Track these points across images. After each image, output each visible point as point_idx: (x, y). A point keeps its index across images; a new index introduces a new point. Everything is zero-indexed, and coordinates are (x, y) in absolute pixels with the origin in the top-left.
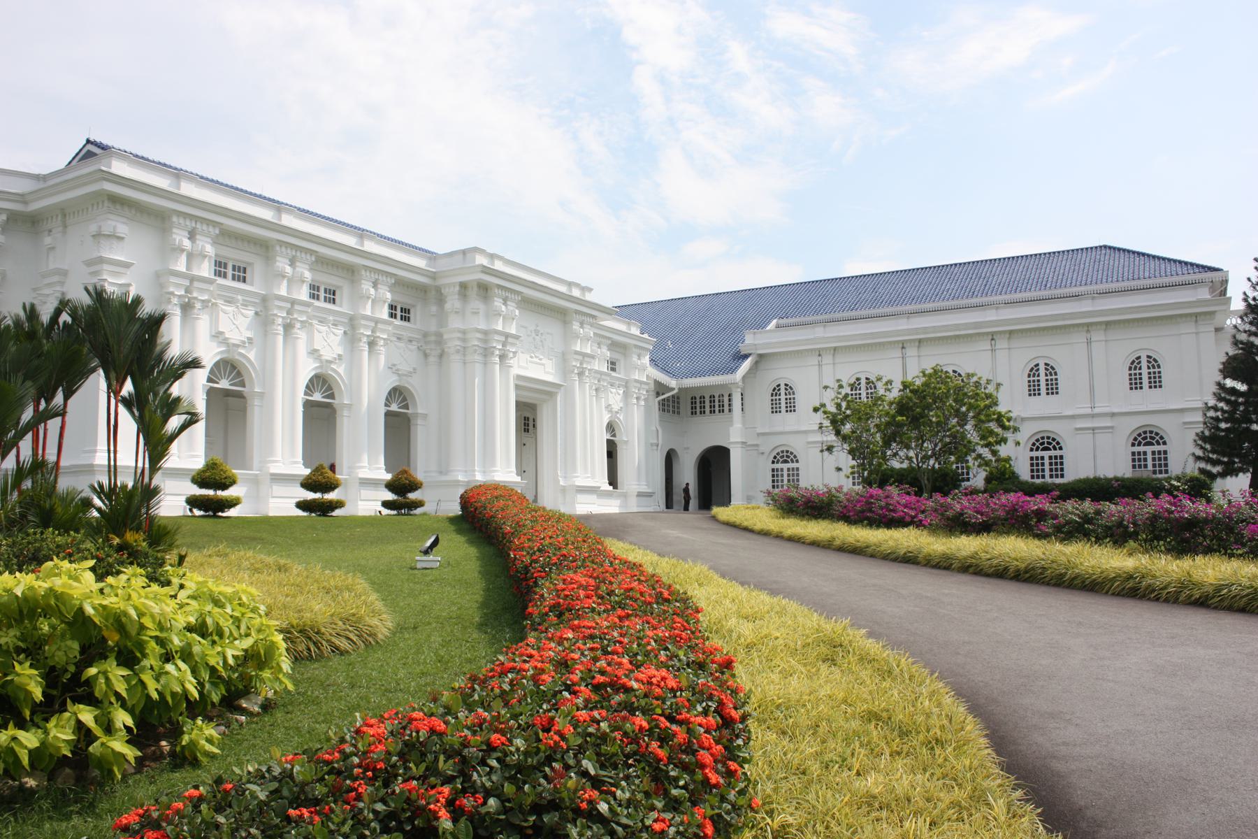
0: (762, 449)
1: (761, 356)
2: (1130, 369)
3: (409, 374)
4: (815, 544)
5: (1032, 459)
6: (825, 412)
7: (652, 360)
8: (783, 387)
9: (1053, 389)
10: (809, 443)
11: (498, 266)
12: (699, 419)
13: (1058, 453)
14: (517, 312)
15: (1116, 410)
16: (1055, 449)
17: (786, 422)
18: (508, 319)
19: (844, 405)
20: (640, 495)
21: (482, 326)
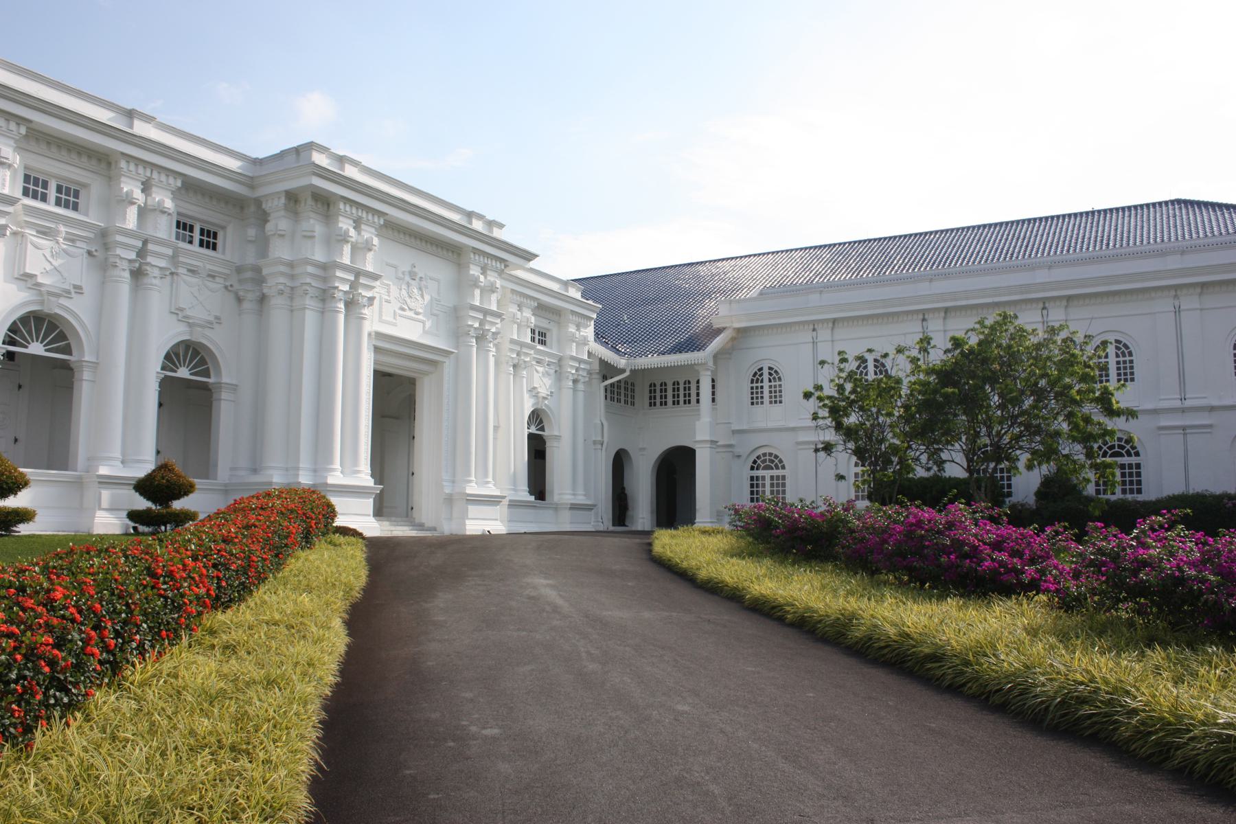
0: (737, 450)
1: (739, 330)
2: (752, 382)
3: (209, 325)
4: (807, 627)
6: (820, 399)
7: (597, 334)
8: (766, 372)
10: (798, 443)
11: (350, 172)
12: (658, 411)
14: (376, 241)
15: (1215, 403)
17: (768, 416)
18: (370, 252)
19: (849, 387)
20: (574, 507)
21: (319, 256)
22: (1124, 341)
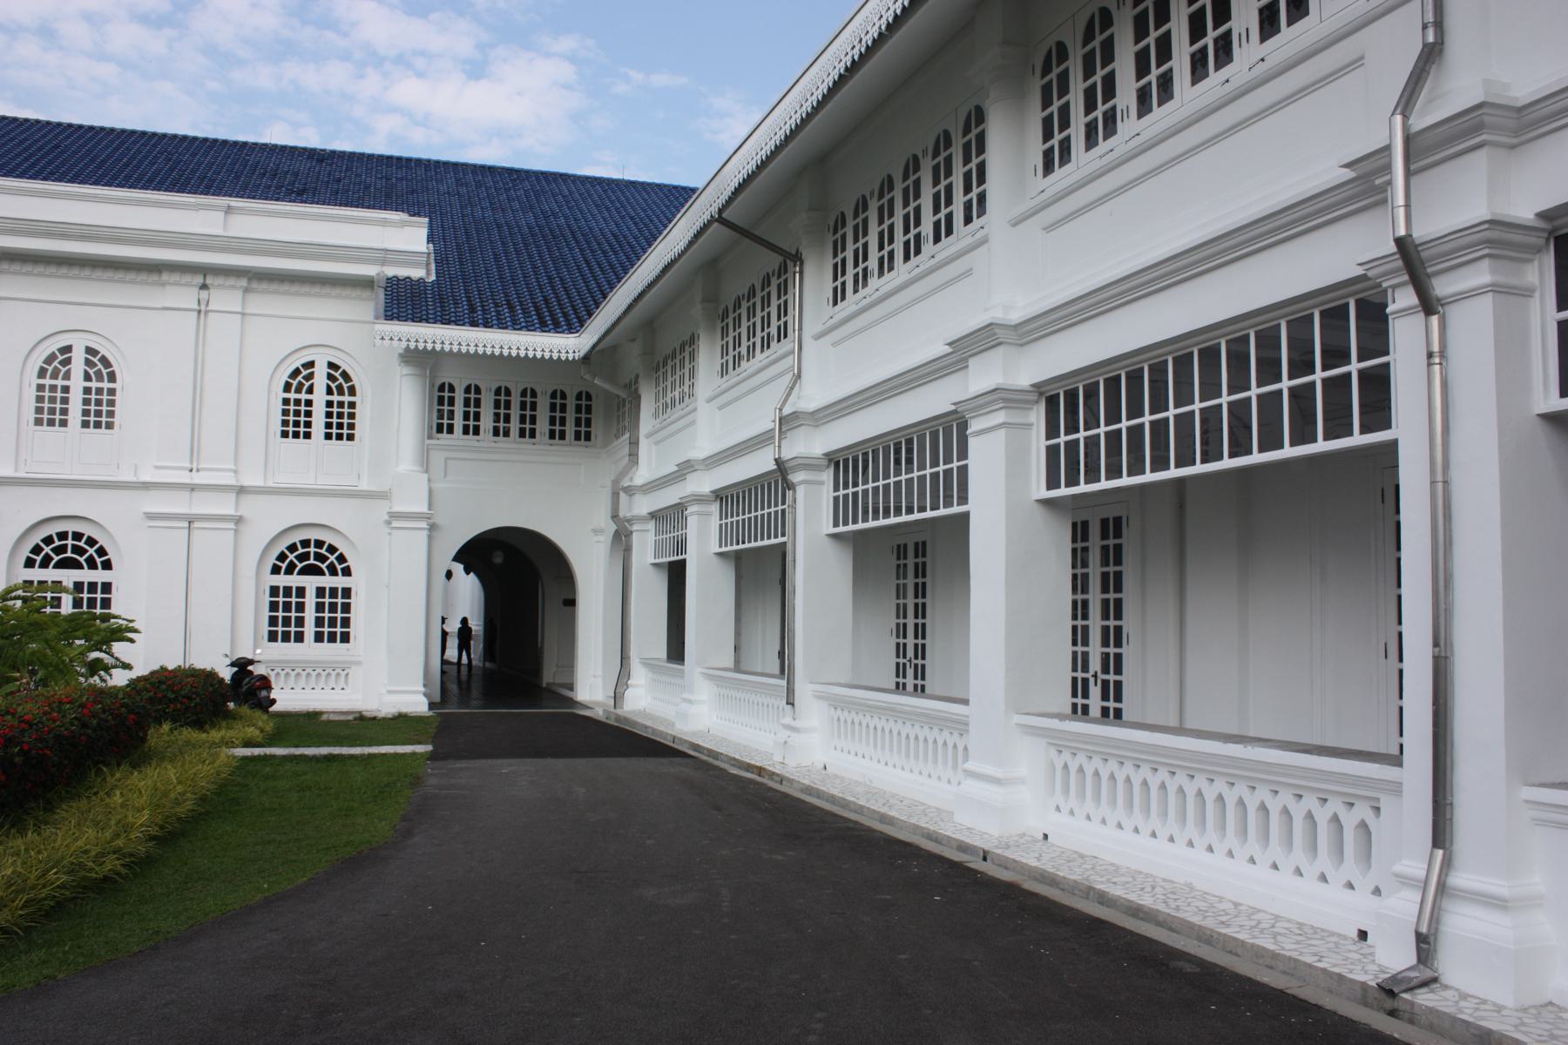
2: (287, 387)
5: (274, 591)
8: (321, 372)
9: (341, 427)
13: (99, 576)
16: (92, 564)
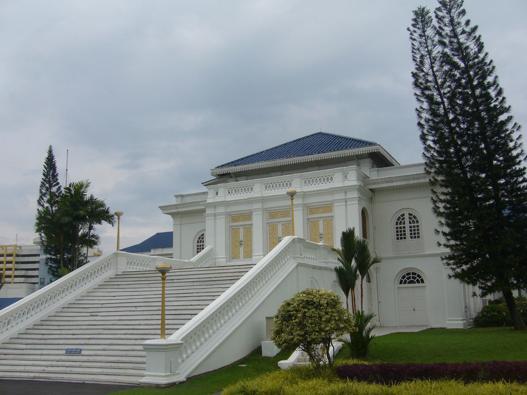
2: (397, 224)
8: (407, 217)
22: (414, 214)
